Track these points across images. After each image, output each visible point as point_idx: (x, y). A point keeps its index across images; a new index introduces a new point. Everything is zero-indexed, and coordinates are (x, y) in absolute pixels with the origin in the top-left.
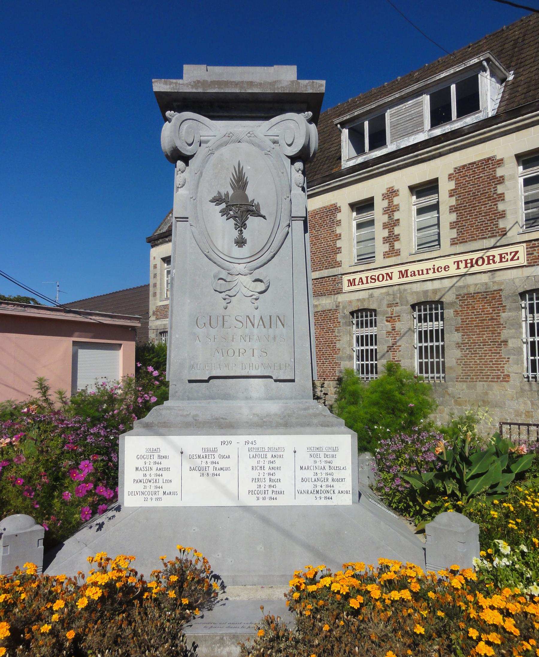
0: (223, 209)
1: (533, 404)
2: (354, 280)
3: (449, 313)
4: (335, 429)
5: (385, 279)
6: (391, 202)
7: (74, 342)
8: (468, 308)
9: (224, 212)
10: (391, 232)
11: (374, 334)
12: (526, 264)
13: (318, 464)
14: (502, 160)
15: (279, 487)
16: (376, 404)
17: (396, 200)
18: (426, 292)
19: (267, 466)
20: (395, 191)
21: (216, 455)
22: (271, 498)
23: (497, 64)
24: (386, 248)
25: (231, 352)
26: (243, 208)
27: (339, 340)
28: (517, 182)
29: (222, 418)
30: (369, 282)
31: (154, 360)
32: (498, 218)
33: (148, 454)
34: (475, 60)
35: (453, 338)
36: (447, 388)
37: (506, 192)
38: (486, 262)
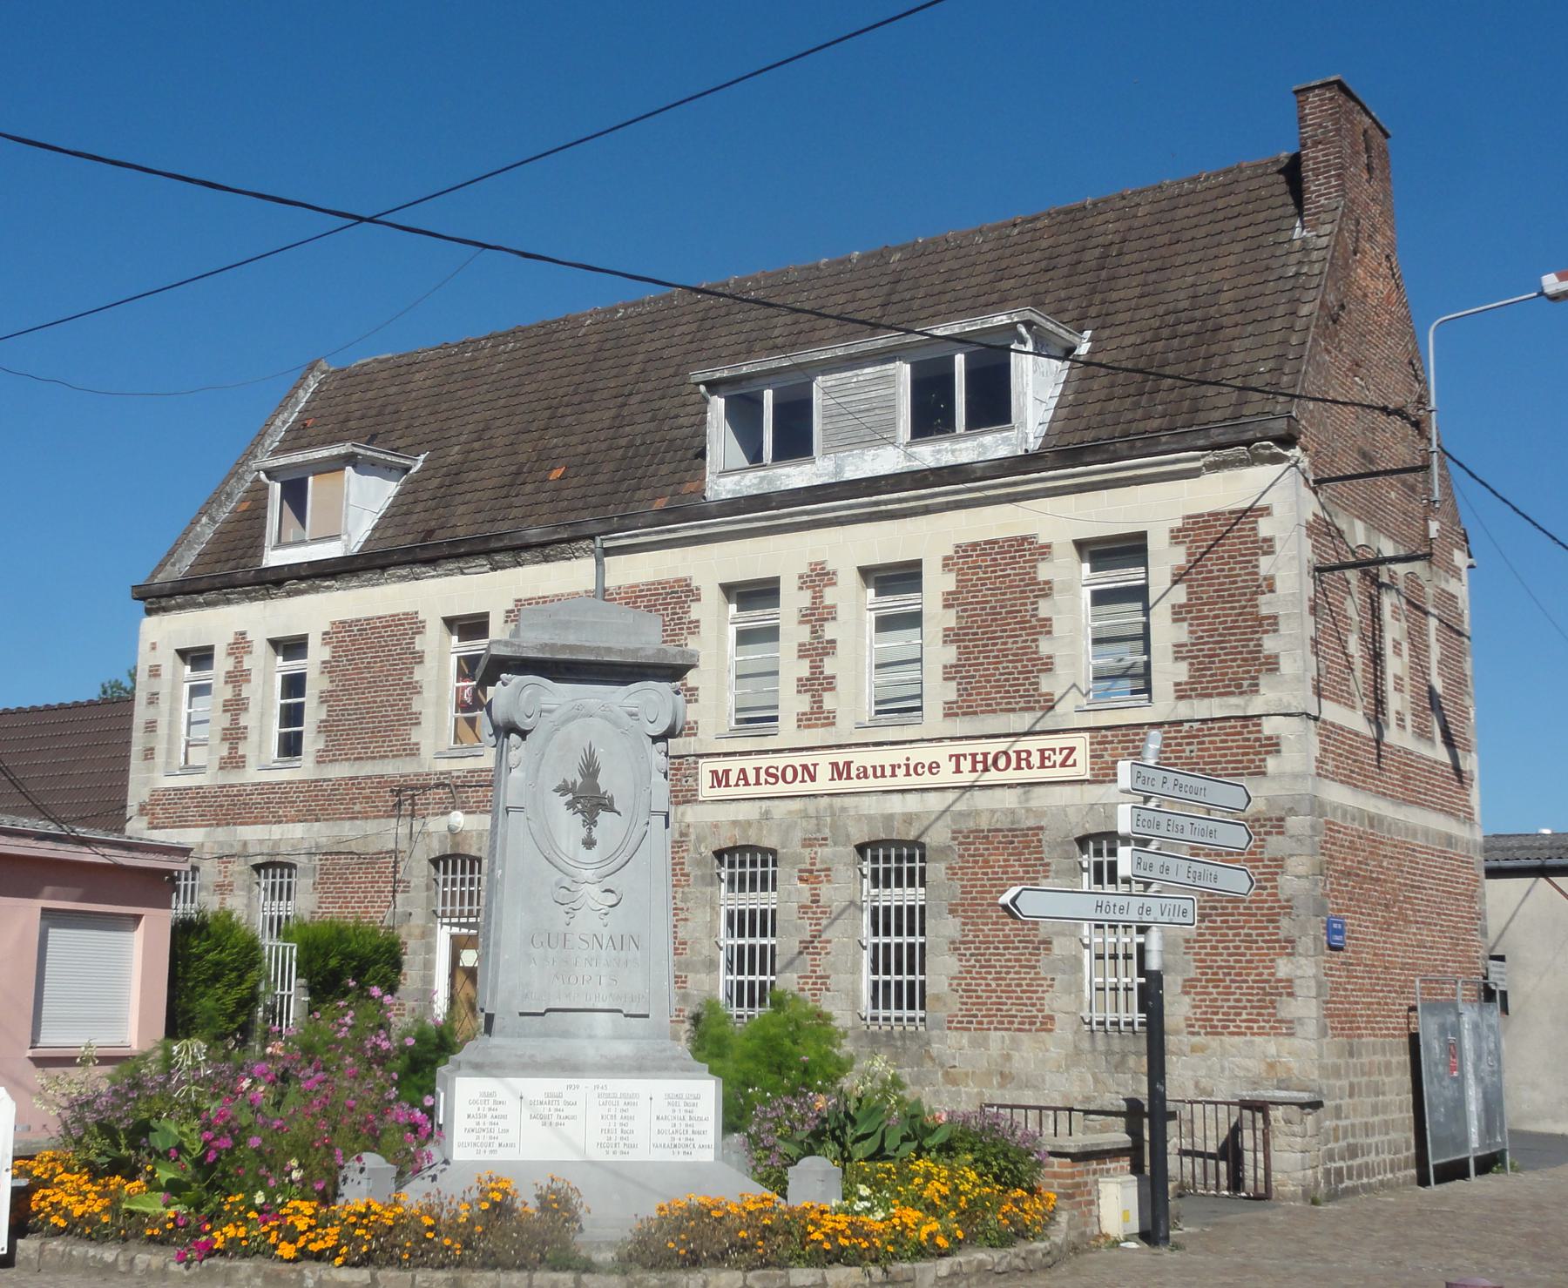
1: (1096, 1080)
2: (727, 772)
3: (936, 870)
5: (800, 778)
6: (817, 597)
7: (46, 912)
8: (976, 862)
9: (570, 805)
10: (816, 668)
11: (769, 907)
12: (1087, 777)
14: (1048, 546)
15: (632, 1139)
16: (753, 1056)
17: (830, 595)
18: (889, 818)
19: (619, 1115)
23: (1050, 326)
24: (804, 703)
25: (573, 980)
26: (595, 801)
27: (686, 920)
28: (1078, 596)
31: (210, 956)
32: (1040, 671)
34: (1001, 319)
35: (943, 928)
36: (928, 1043)
37: (1054, 617)
38: (1013, 764)
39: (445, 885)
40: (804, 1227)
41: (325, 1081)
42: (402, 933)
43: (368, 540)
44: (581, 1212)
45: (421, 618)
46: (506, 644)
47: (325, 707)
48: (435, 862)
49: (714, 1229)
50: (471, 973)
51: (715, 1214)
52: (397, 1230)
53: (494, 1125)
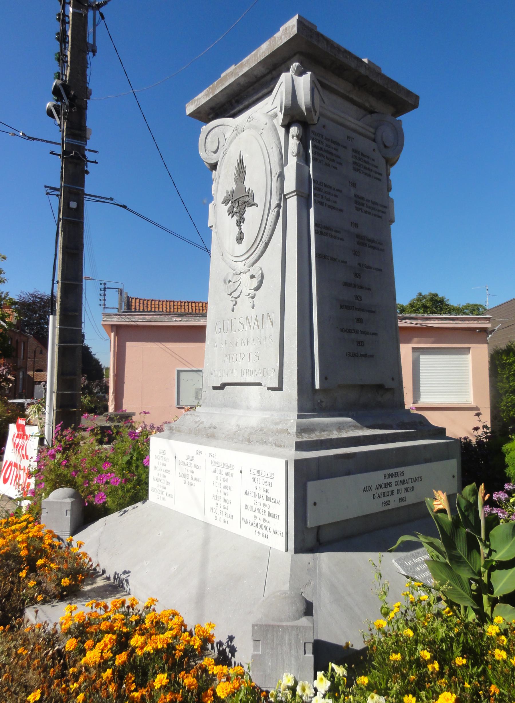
7: (413, 348)
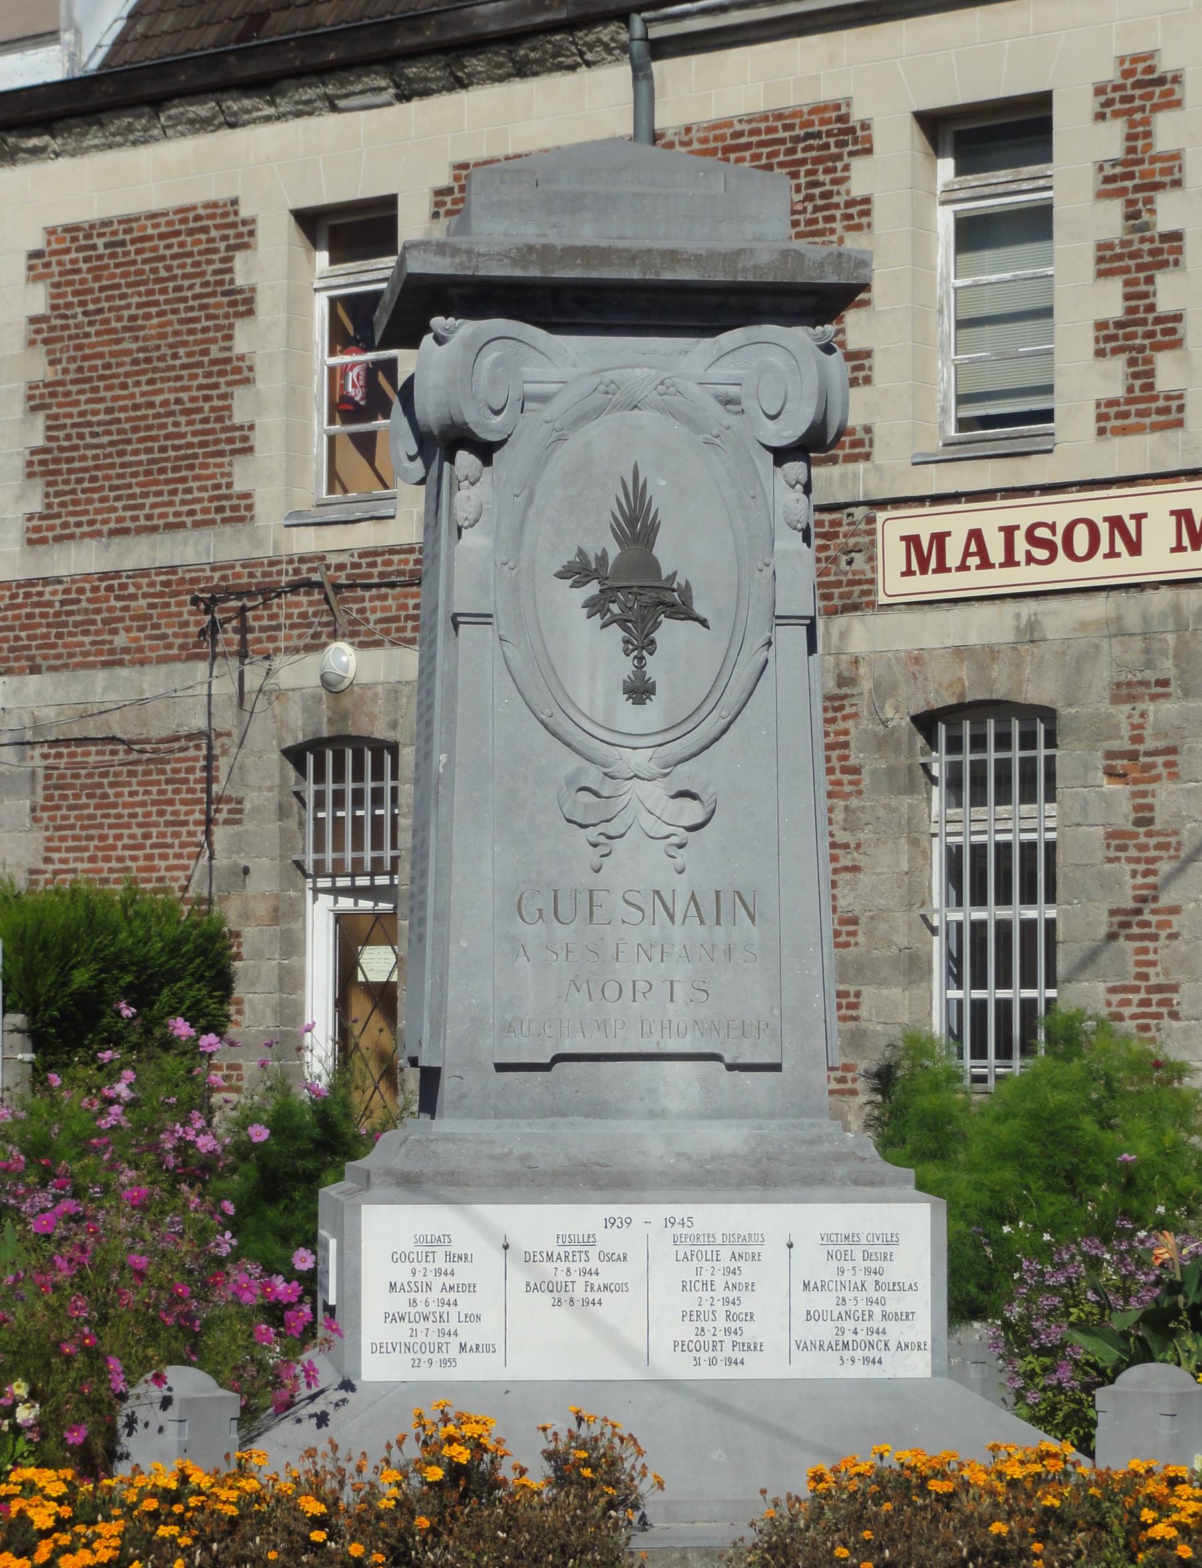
0: (593, 598)
2: (939, 539)
4: (890, 1191)
5: (1104, 547)
6: (1138, 135)
9: (594, 607)
10: (1138, 297)
13: (848, 1276)
15: (751, 1332)
16: (1012, 1155)
20: (1161, 81)
21: (593, 1252)
22: (730, 1362)
24: (1111, 378)
27: (855, 869)
29: (597, 1164)
30: (1020, 556)
33: (420, 1249)
39: (320, 804)
40: (1134, 1514)
41: (77, 1218)
42: (230, 912)
43: (120, 42)
44: (644, 1486)
45: (245, 212)
46: (441, 248)
47: (40, 419)
48: (295, 755)
49: (935, 1519)
50: (384, 997)
51: (935, 1486)
52: (247, 1528)
53: (454, 1305)
